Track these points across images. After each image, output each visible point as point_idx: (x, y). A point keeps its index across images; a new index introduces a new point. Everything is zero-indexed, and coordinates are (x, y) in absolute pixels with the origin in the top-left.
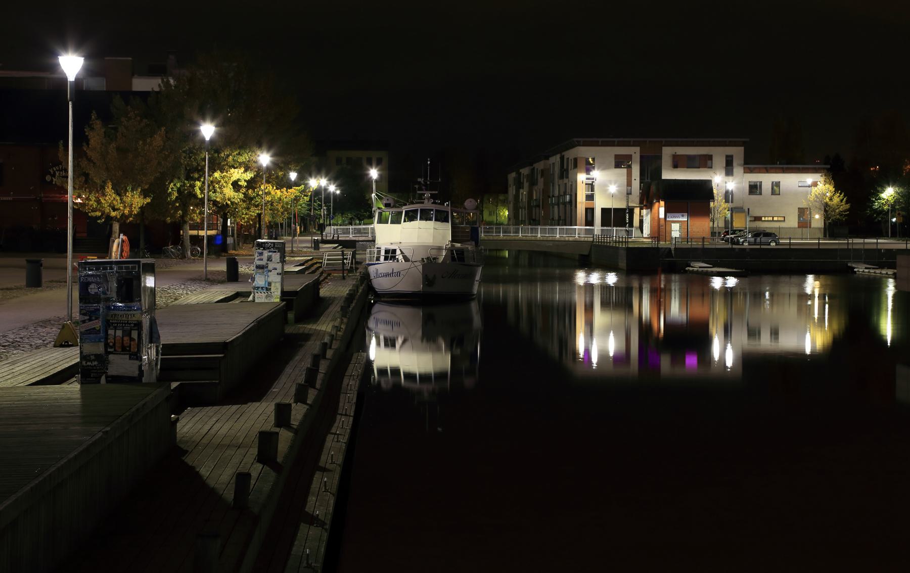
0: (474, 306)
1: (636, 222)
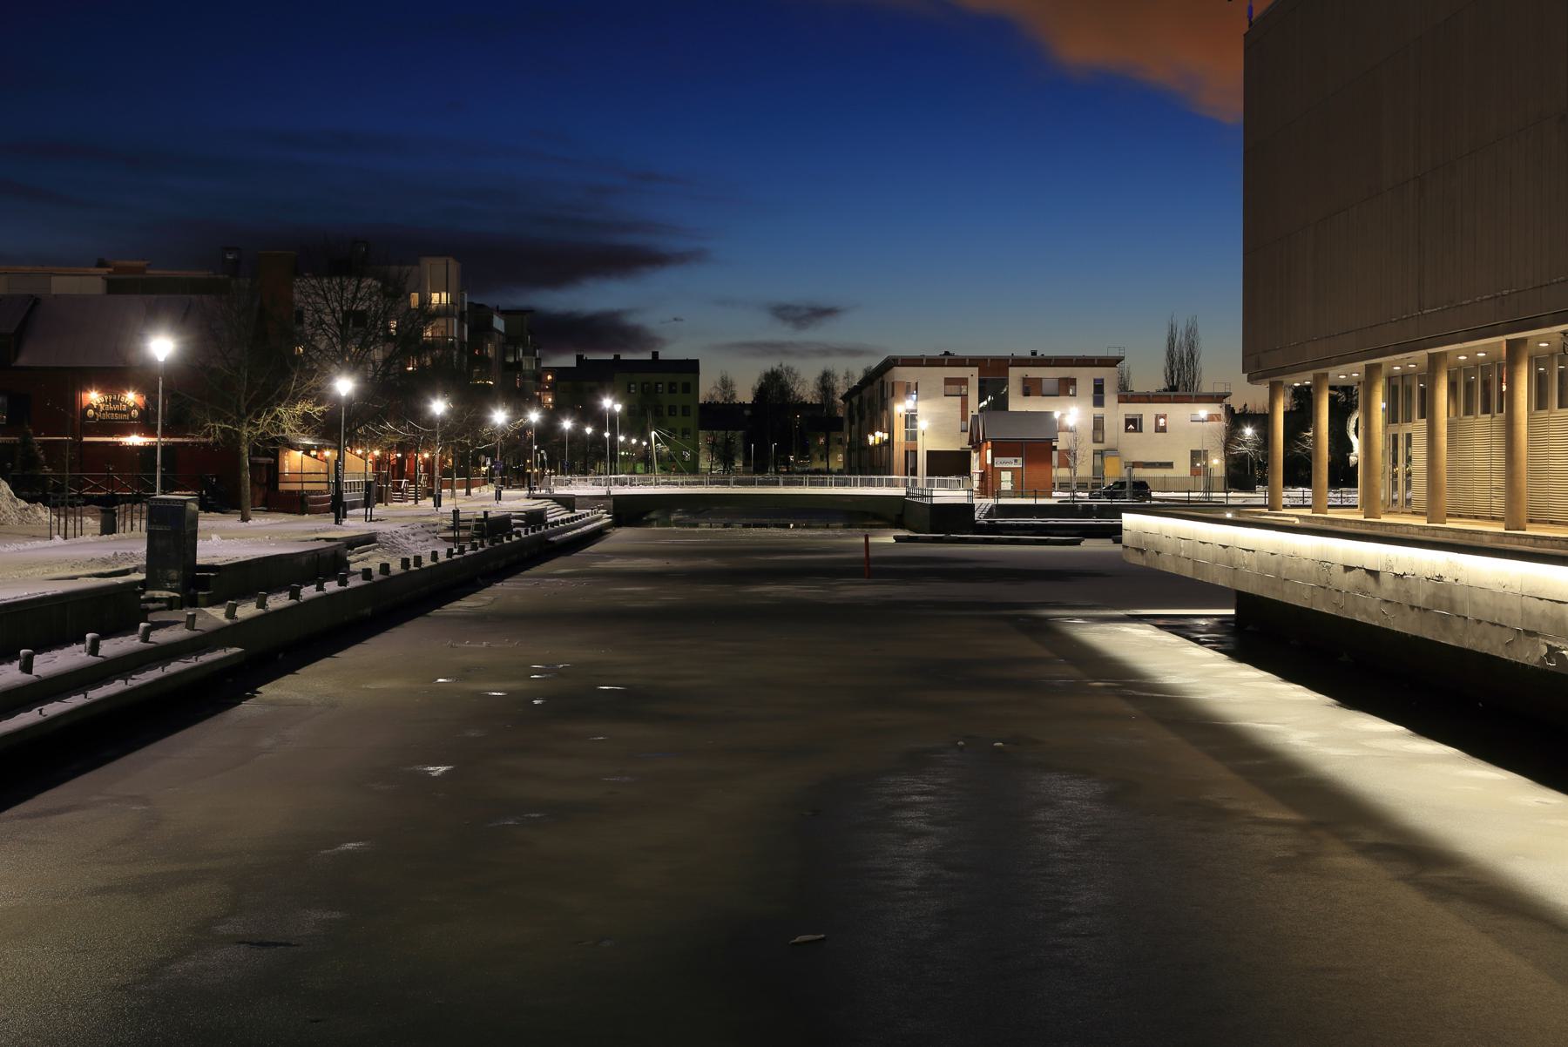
0: (26, 473)
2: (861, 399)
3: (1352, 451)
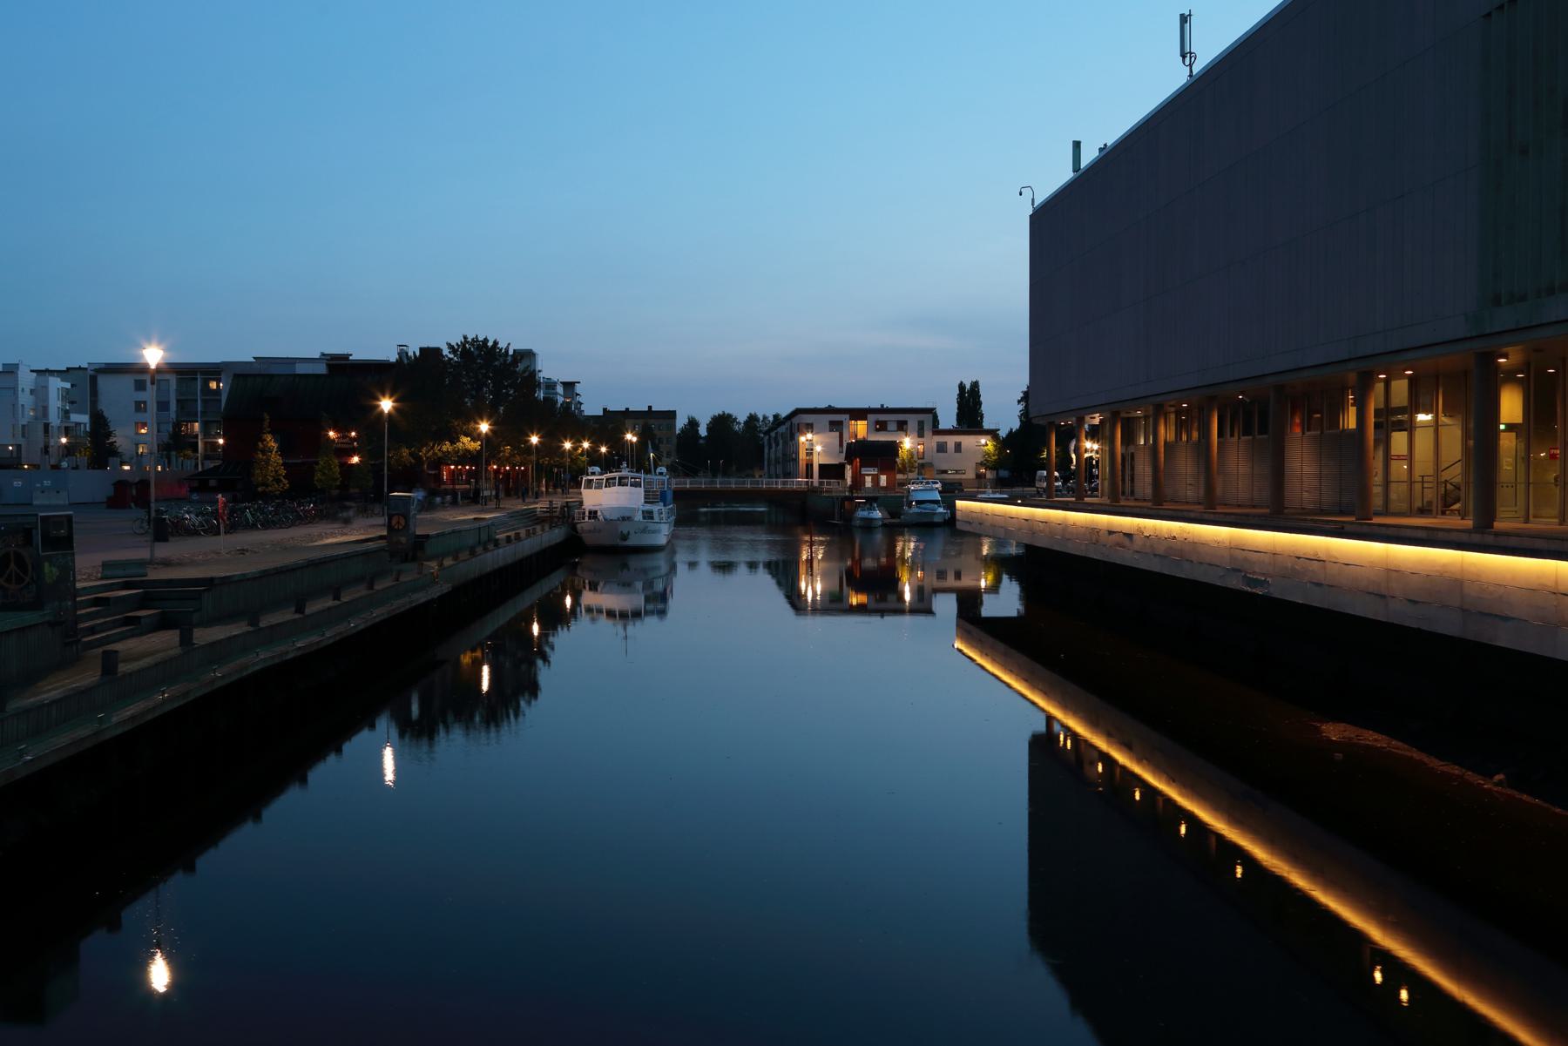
2: (776, 433)
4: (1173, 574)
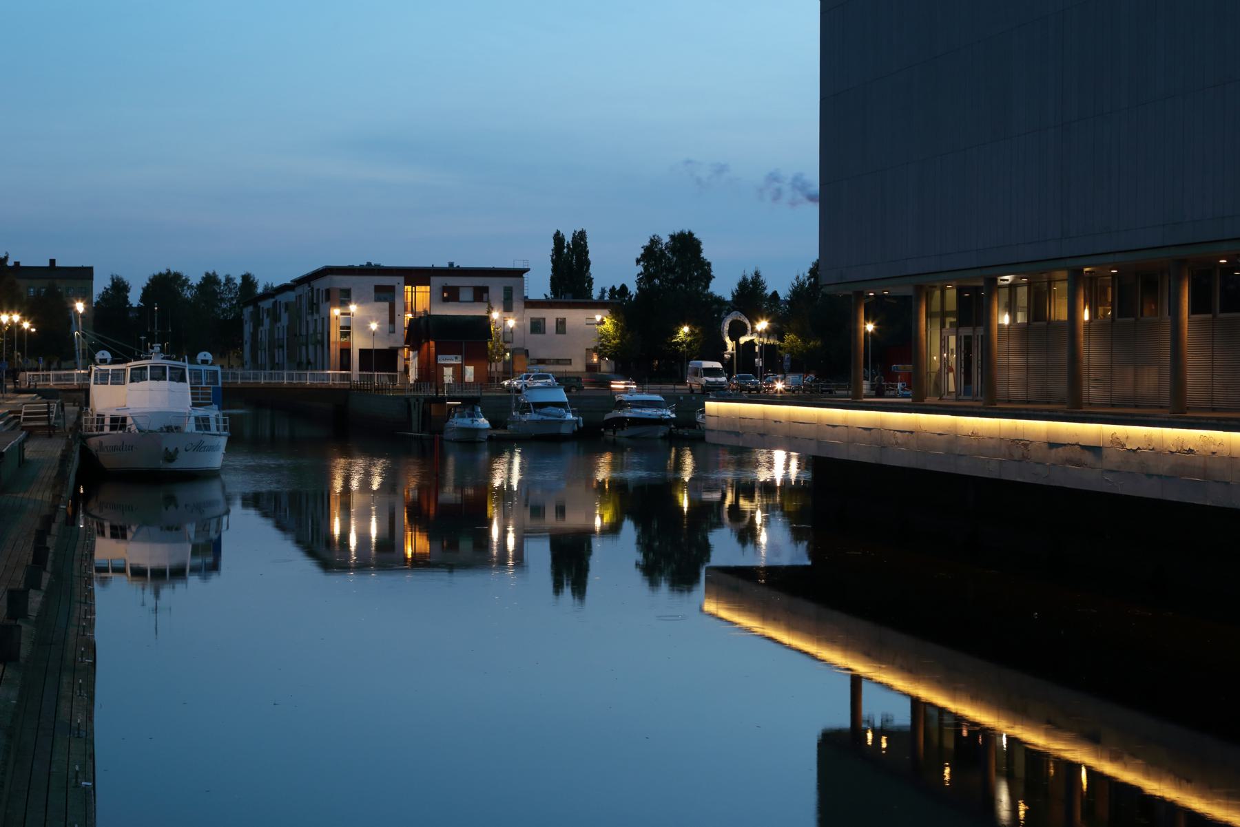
1: (400, 367)
3: (726, 350)
4: (1192, 502)
